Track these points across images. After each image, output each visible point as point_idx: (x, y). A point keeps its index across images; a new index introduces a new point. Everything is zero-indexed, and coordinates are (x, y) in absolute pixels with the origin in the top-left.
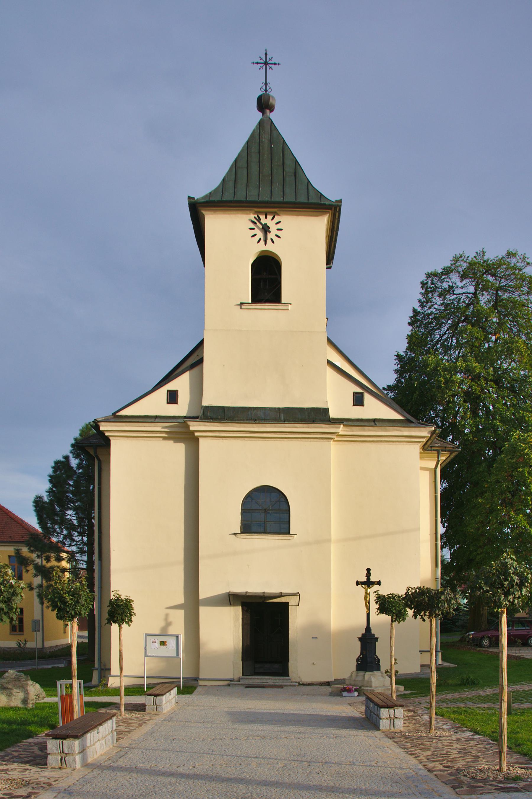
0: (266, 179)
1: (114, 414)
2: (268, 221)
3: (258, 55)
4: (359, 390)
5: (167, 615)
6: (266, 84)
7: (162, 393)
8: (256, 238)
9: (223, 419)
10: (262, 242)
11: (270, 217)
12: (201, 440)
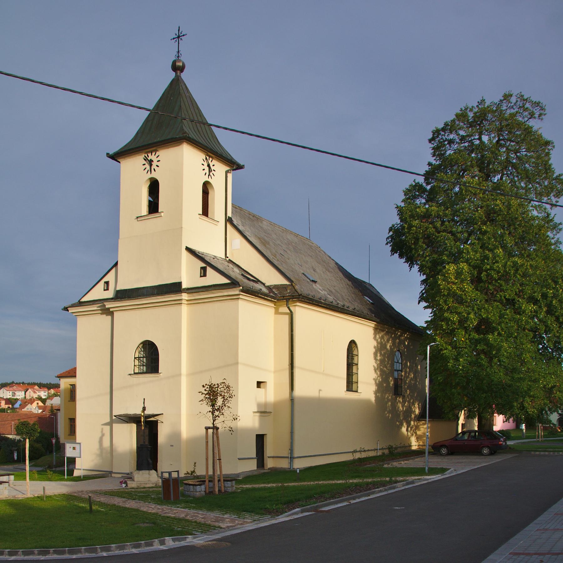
0: (172, 121)
1: (79, 301)
2: (151, 157)
3: (174, 33)
4: (205, 265)
5: (102, 429)
6: (178, 52)
7: (101, 285)
8: (146, 170)
9: (125, 298)
10: (149, 172)
11: (154, 154)
12: (115, 313)
